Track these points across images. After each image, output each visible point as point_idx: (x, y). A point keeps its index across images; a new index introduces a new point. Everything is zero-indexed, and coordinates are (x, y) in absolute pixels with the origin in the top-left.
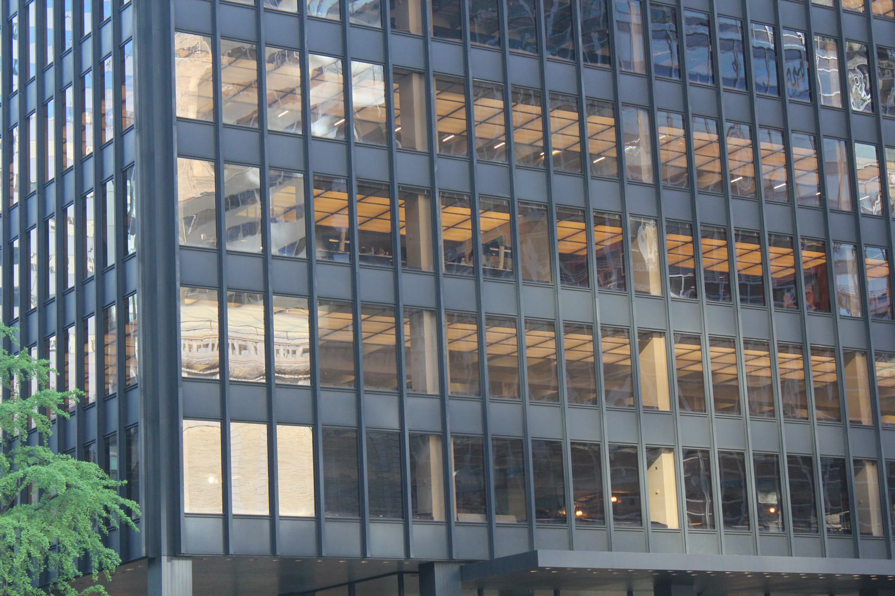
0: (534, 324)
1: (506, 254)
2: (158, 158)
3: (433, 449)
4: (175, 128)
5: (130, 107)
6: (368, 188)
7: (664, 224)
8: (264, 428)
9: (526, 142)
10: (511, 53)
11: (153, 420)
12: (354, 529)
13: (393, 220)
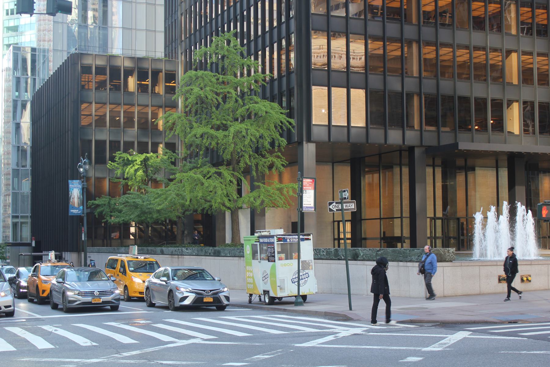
7: (519, 3)
11: (300, 86)
12: (382, 132)
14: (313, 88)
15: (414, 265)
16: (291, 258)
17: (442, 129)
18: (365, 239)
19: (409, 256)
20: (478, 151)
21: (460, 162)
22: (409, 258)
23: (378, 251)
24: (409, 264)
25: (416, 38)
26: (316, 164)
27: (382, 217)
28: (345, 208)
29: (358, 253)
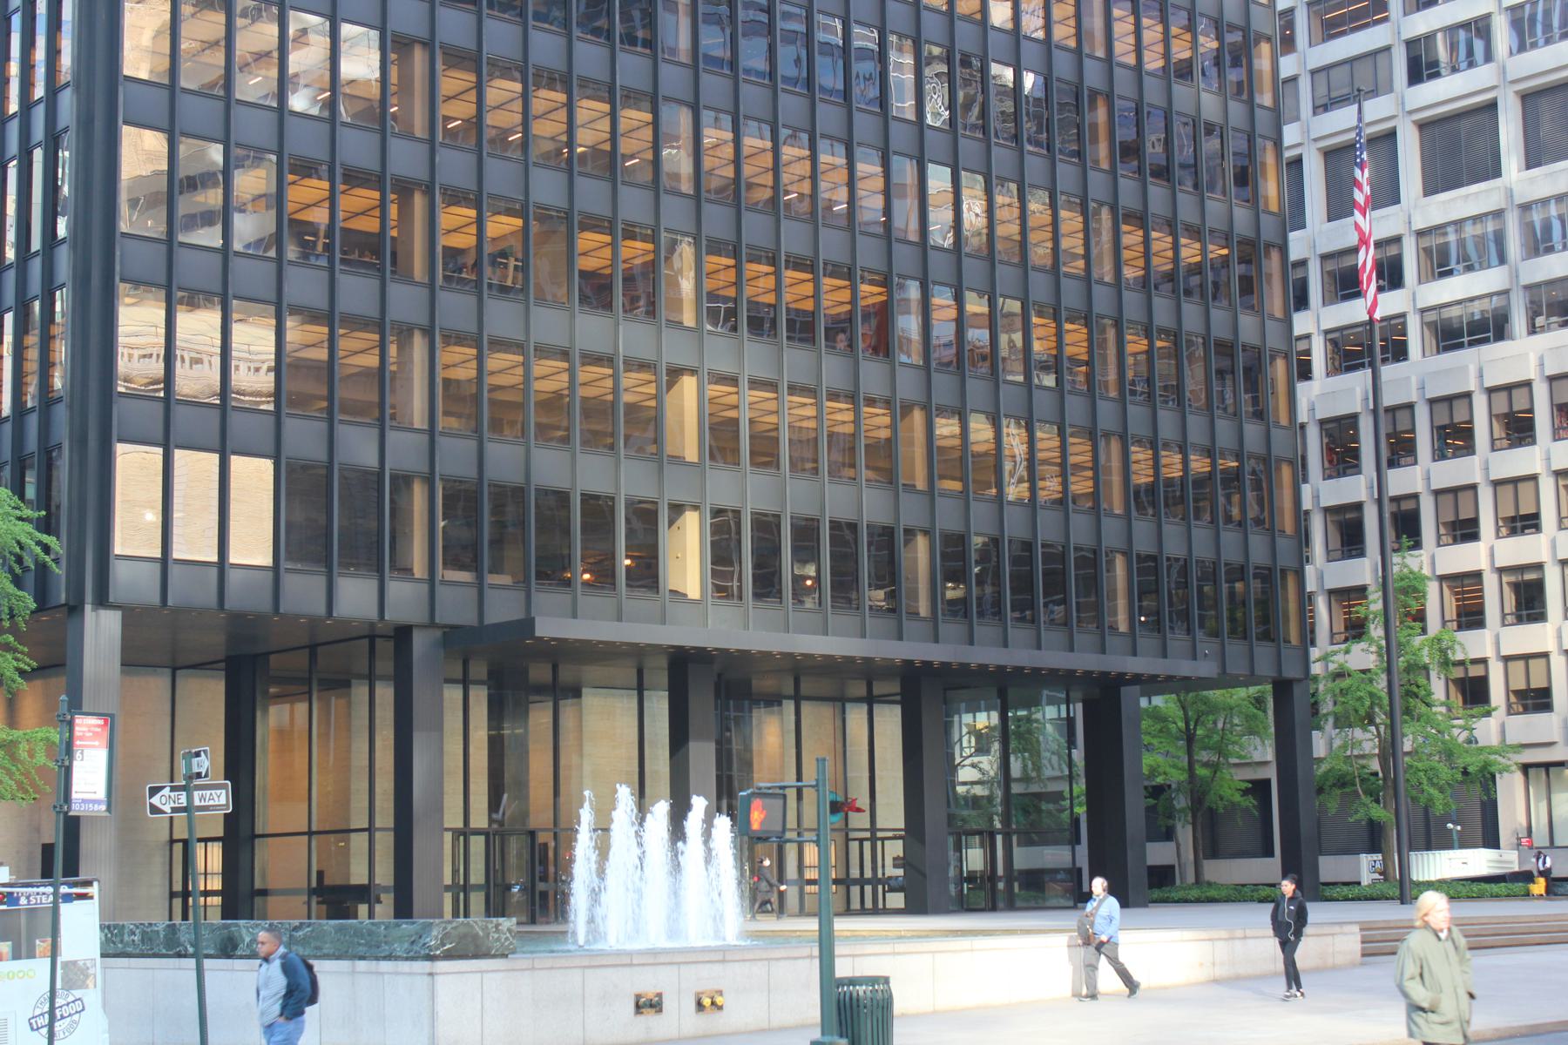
0: (544, 352)
1: (516, 267)
2: (99, 126)
3: (419, 493)
4: (121, 89)
5: (66, 60)
6: (355, 178)
7: (704, 243)
9: (548, 135)
11: (80, 441)
12: (319, 582)
13: (383, 218)
14: (121, 449)
15: (400, 969)
16: (31, 955)
18: (264, 893)
19: (386, 943)
21: (539, 673)
23: (296, 929)
24: (385, 966)
25: (423, 320)
26: (122, 672)
27: (314, 828)
28: (197, 803)
29: (236, 934)
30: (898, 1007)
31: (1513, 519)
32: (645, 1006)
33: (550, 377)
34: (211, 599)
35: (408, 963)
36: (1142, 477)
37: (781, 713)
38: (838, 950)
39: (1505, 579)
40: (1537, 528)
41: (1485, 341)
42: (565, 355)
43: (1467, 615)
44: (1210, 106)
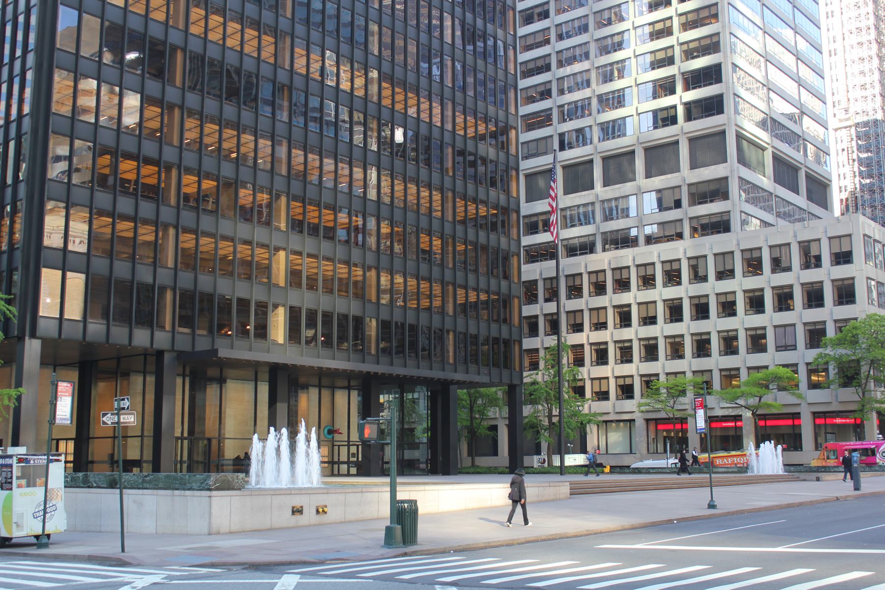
0: (225, 238)
1: (213, 202)
2: (41, 132)
3: (169, 295)
4: (51, 118)
6: (148, 161)
7: (291, 196)
8: (60, 273)
10: (207, 97)
11: (26, 267)
12: (126, 331)
16: (35, 485)
17: (198, 332)
18: (92, 462)
20: (239, 360)
21: (212, 372)
22: (189, 486)
23: (146, 476)
24: (188, 493)
25: (174, 222)
26: (41, 367)
28: (122, 420)
30: (420, 511)
31: (597, 324)
32: (296, 511)
33: (225, 248)
34: (80, 336)
35: (199, 492)
36: (461, 300)
37: (308, 393)
38: (398, 489)
39: (642, 343)
40: (606, 328)
41: (586, 253)
42: (232, 240)
43: (578, 361)
44: (492, 153)
